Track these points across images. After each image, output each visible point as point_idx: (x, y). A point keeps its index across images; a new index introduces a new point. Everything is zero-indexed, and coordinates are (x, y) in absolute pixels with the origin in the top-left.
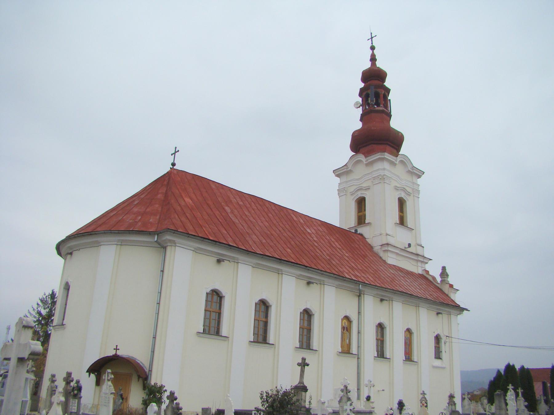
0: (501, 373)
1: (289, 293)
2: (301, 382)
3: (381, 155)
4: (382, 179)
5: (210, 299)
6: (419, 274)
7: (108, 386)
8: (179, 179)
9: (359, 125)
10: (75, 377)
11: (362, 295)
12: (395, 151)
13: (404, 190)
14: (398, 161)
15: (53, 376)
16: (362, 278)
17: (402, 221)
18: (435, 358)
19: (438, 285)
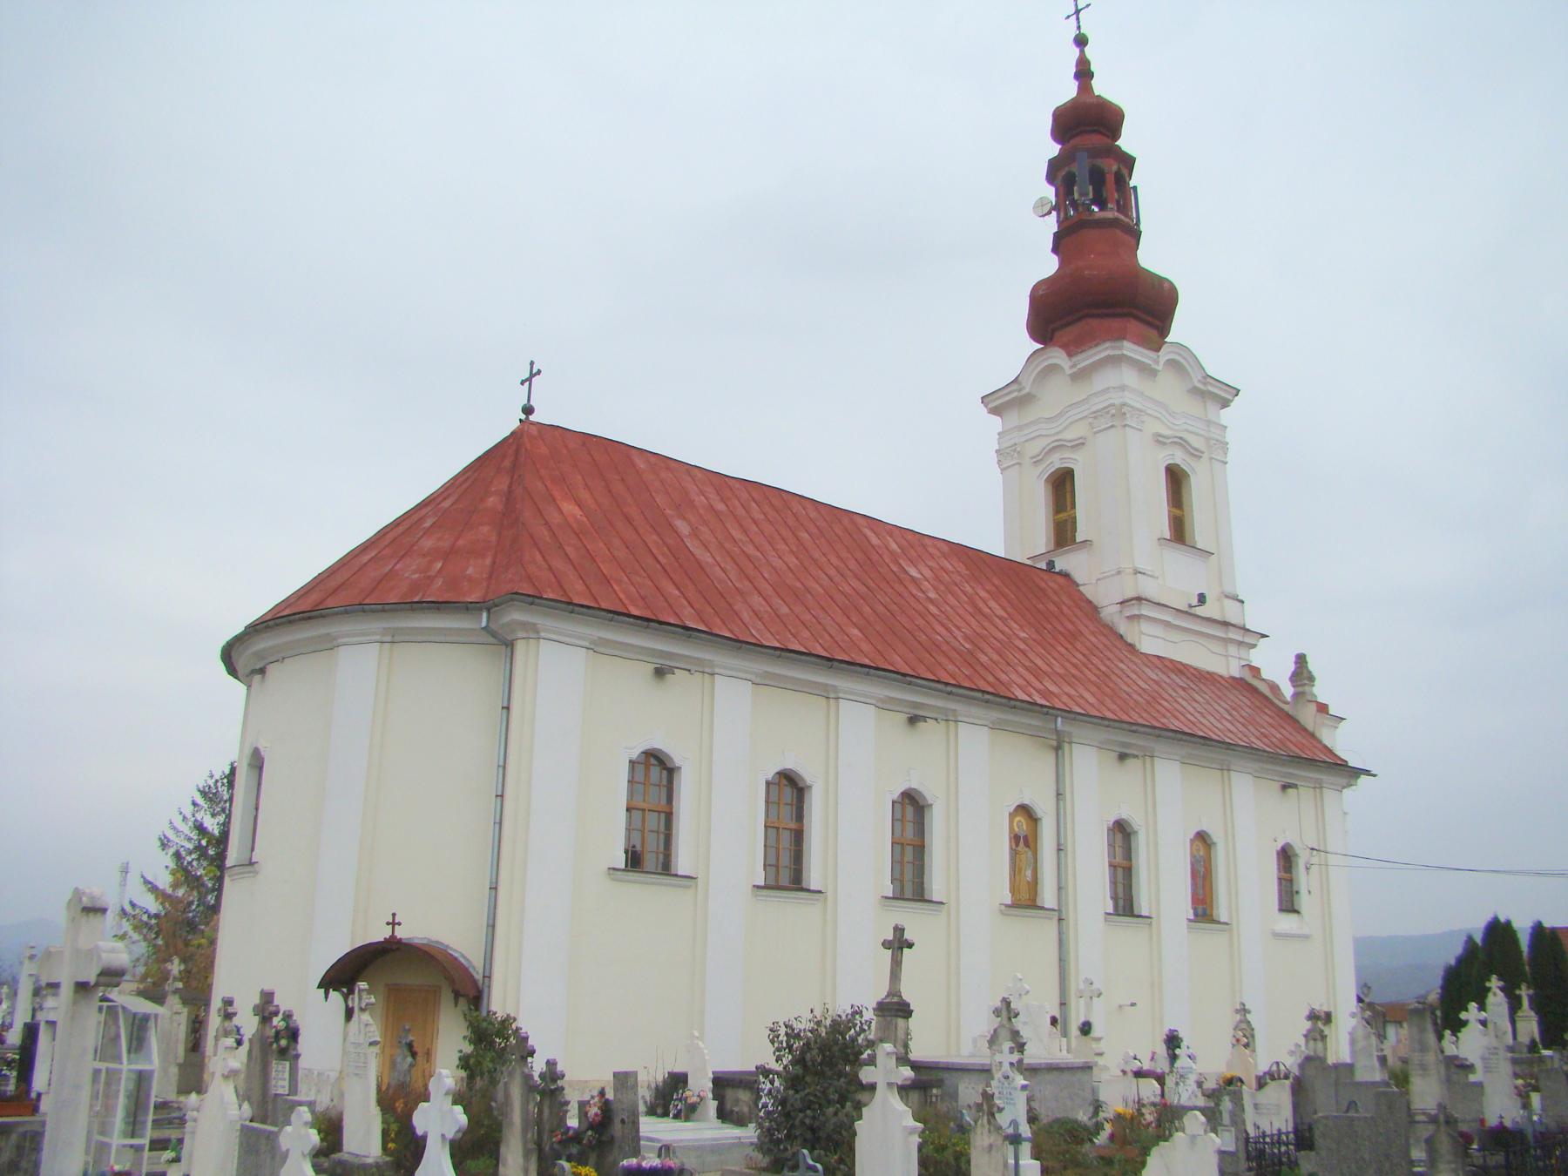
0: (1475, 944)
1: (859, 751)
2: (894, 992)
3: (1113, 348)
4: (1118, 415)
5: (640, 776)
6: (1233, 678)
7: (369, 1025)
8: (544, 450)
9: (1049, 265)
10: (283, 1002)
11: (1066, 747)
12: (1153, 334)
13: (1181, 443)
14: (1163, 360)
15: (228, 1002)
16: (1065, 699)
17: (1179, 532)
18: (1281, 910)
19: (1286, 707)
